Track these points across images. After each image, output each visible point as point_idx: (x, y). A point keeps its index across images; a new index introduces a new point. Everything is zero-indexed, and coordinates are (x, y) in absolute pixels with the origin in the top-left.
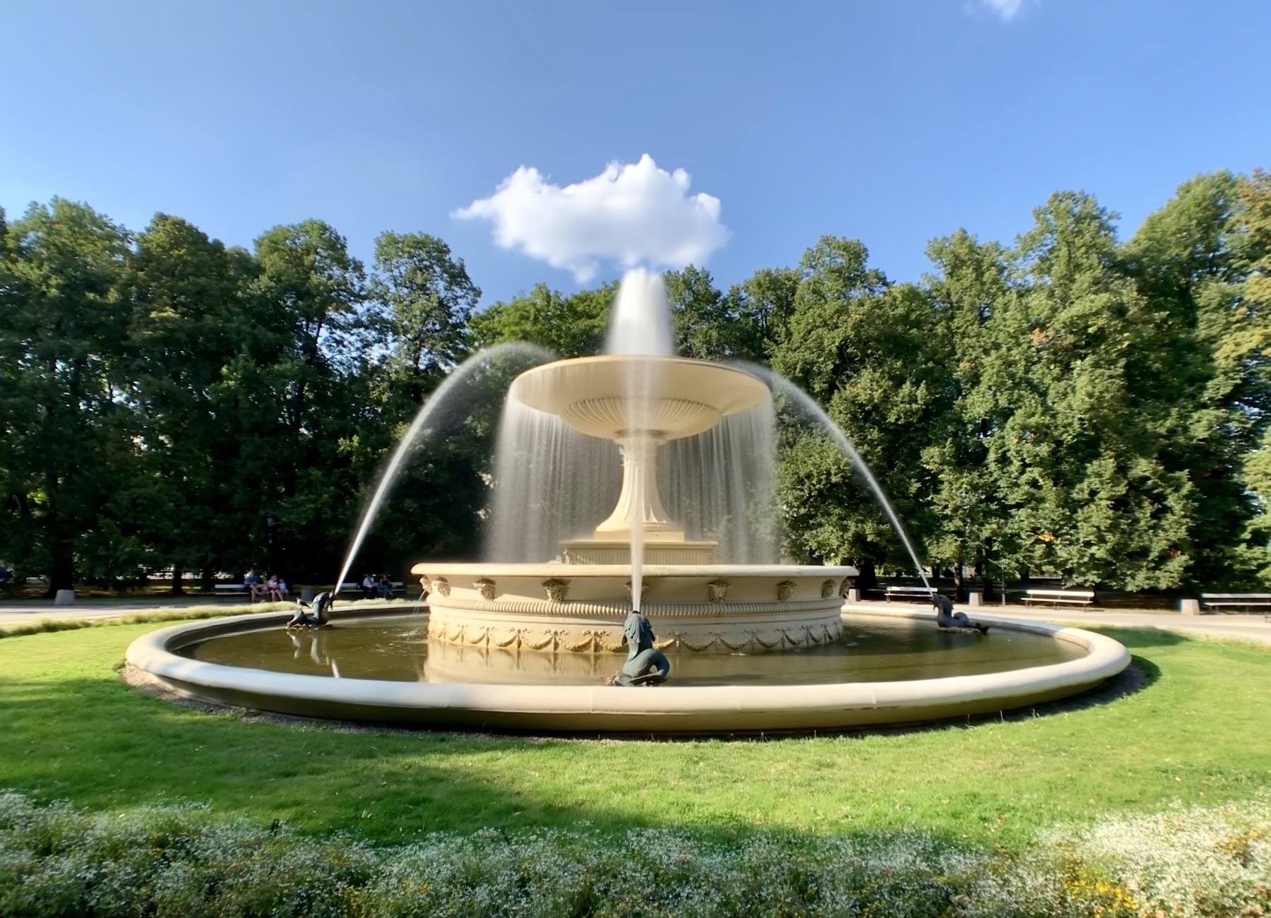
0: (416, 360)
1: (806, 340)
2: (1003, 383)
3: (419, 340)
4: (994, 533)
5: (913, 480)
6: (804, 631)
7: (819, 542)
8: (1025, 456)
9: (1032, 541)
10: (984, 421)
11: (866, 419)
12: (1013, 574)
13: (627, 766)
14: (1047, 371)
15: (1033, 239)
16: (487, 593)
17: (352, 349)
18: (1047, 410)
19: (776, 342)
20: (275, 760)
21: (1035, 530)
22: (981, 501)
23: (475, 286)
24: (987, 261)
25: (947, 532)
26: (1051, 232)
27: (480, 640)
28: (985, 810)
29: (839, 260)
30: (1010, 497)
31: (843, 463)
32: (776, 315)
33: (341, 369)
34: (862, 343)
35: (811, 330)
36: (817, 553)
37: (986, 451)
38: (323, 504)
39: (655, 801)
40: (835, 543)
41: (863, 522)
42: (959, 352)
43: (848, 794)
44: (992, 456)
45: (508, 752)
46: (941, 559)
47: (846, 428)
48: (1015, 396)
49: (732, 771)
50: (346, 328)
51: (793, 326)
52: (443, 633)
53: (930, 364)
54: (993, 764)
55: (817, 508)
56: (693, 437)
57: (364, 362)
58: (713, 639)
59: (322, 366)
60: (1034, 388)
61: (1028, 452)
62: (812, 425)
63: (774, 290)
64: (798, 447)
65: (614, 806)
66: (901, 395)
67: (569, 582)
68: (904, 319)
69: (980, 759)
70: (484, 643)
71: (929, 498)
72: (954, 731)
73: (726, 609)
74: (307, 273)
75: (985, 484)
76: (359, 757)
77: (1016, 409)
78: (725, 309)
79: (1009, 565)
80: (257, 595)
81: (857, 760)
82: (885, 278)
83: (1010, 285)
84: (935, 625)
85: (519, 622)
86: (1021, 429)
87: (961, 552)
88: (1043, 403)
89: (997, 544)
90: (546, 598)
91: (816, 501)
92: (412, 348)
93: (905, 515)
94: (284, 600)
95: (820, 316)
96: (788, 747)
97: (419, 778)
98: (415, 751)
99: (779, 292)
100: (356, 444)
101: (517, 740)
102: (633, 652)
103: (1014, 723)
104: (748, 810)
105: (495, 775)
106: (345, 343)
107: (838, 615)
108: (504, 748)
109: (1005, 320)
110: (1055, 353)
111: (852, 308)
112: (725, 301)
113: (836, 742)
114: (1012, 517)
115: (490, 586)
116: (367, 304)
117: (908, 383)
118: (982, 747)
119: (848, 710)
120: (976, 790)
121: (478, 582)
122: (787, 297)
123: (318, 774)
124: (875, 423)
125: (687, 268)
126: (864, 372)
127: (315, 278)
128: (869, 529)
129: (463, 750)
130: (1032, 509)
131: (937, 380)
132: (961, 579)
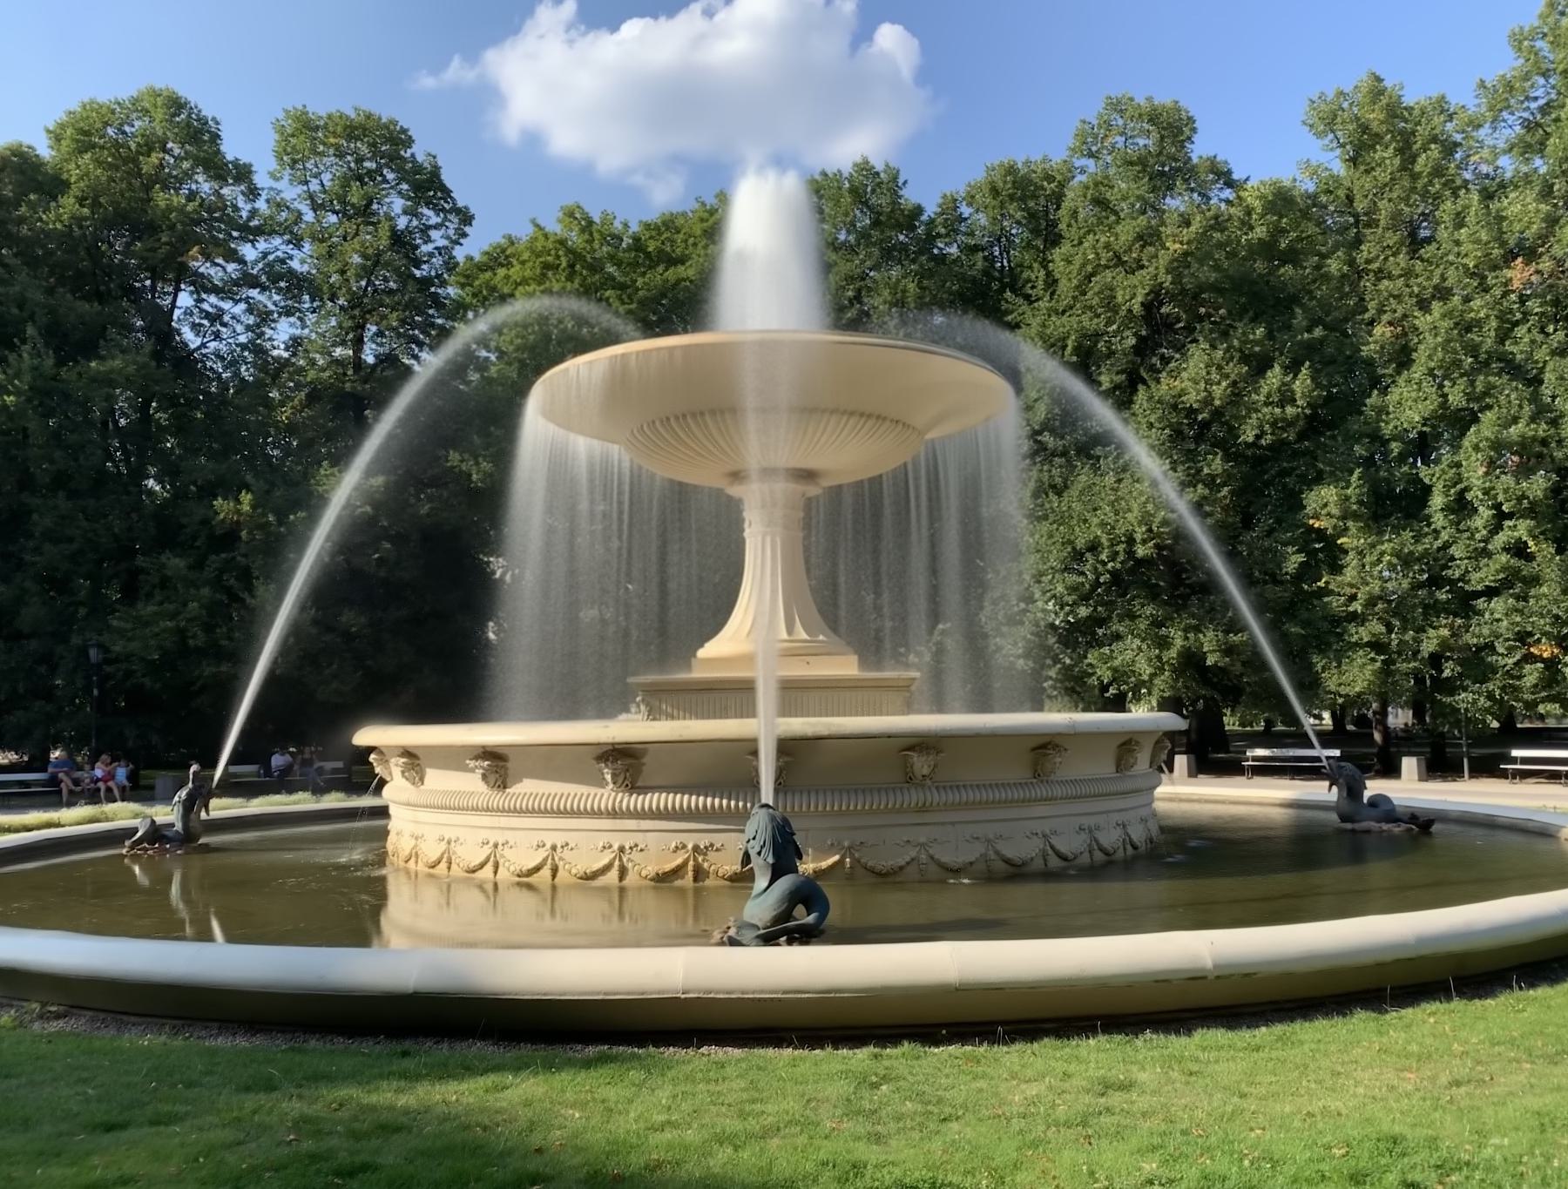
0: (358, 343)
1: (1084, 293)
2: (1457, 364)
3: (359, 312)
4: (1444, 644)
5: (1290, 549)
6: (1084, 836)
7: (1115, 670)
8: (1501, 498)
9: (1518, 657)
10: (1421, 434)
11: (1198, 439)
12: (1484, 721)
13: (745, 1096)
14: (1539, 338)
15: (1510, 87)
16: (492, 778)
17: (239, 328)
18: (1541, 411)
19: (1027, 297)
20: (88, 1100)
21: (1523, 637)
22: (1421, 585)
23: (460, 204)
24: (1422, 131)
25: (1356, 644)
26: (1545, 74)
27: (482, 866)
28: (1414, 1167)
29: (1141, 142)
30: (1475, 576)
31: (1157, 521)
32: (1029, 246)
33: (219, 367)
34: (1190, 298)
35: (1093, 275)
36: (1112, 691)
37: (1427, 490)
38: (189, 620)
39: (793, 1160)
40: (1144, 669)
41: (1197, 629)
42: (1372, 306)
43: (1156, 1140)
44: (1437, 501)
45: (524, 1074)
46: (1347, 695)
47: (1161, 455)
48: (1480, 387)
49: (940, 1101)
50: (225, 291)
51: (1058, 267)
52: (414, 855)
53: (1318, 332)
54: (1433, 1079)
55: (1110, 605)
56: (872, 480)
57: (259, 351)
58: (913, 853)
59: (185, 363)
60: (1513, 369)
61: (1506, 491)
62: (1098, 451)
63: (1023, 199)
64: (1074, 492)
65: (716, 1170)
66: (1265, 390)
67: (644, 752)
68: (1267, 249)
69: (1409, 1070)
70: (487, 872)
71: (1321, 584)
72: (1361, 1021)
73: (935, 797)
74: (148, 188)
75: (1426, 552)
76: (248, 1089)
77: (1481, 411)
78: (931, 238)
79: (1475, 701)
80: (71, 792)
81: (1175, 1075)
82: (1229, 172)
83: (1468, 176)
84: (1333, 817)
85: (554, 831)
86: (1491, 448)
87: (1384, 683)
88: (1535, 398)
89: (1450, 664)
90: (601, 783)
91: (1108, 591)
92: (348, 324)
93: (1277, 614)
94: (123, 800)
95: (1107, 246)
96: (1046, 1054)
97: (356, 1125)
98: (354, 1077)
99: (1031, 204)
100: (246, 508)
101: (542, 1052)
102: (761, 882)
103: (1477, 1002)
104: (966, 1173)
105: (499, 1118)
106: (226, 318)
107: (1150, 804)
108: (518, 1068)
109: (1458, 243)
110: (1556, 303)
111: (1167, 231)
112: (932, 221)
113: (1139, 1042)
114: (1480, 613)
116: (262, 245)
117: (1277, 369)
118: (1414, 1048)
119: (1196, 978)
120: (1397, 1129)
121: (476, 758)
122: (1047, 213)
123: (166, 1125)
124: (1218, 444)
125: (855, 165)
126: (1192, 348)
127: (161, 198)
128: (1209, 642)
129: (444, 1073)
130: (1518, 598)
131: (1332, 362)
132: (1386, 731)
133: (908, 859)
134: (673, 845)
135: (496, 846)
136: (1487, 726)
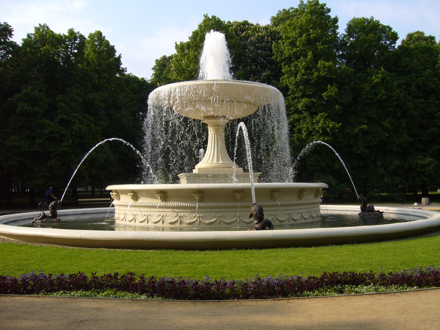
6: (309, 214)
16: (134, 198)
27: (132, 220)
85: (146, 211)
115: (135, 195)
133: (271, 219)
134: (175, 215)
135: (135, 215)
136: (82, 187)
